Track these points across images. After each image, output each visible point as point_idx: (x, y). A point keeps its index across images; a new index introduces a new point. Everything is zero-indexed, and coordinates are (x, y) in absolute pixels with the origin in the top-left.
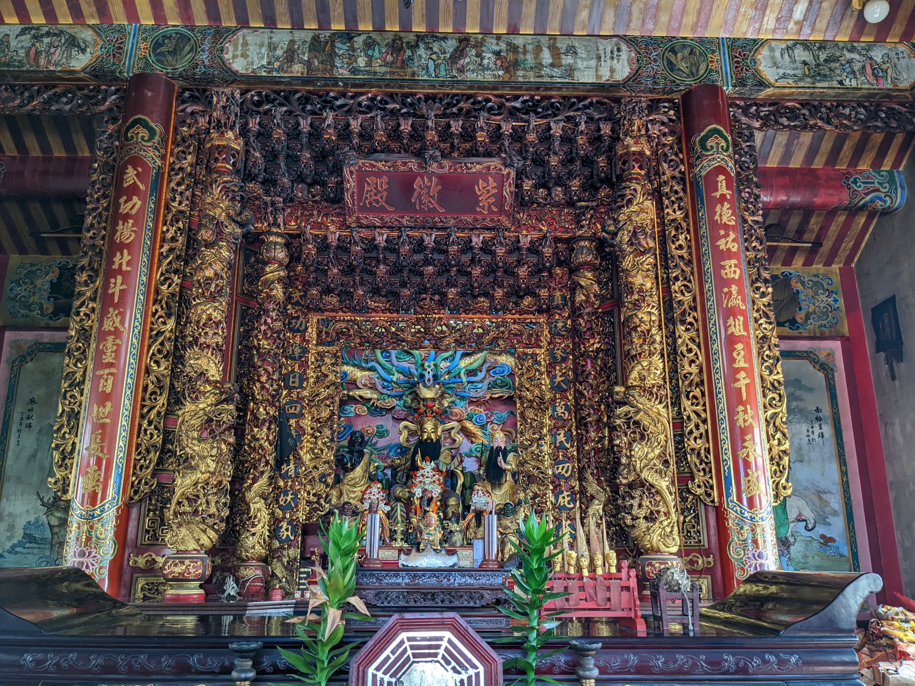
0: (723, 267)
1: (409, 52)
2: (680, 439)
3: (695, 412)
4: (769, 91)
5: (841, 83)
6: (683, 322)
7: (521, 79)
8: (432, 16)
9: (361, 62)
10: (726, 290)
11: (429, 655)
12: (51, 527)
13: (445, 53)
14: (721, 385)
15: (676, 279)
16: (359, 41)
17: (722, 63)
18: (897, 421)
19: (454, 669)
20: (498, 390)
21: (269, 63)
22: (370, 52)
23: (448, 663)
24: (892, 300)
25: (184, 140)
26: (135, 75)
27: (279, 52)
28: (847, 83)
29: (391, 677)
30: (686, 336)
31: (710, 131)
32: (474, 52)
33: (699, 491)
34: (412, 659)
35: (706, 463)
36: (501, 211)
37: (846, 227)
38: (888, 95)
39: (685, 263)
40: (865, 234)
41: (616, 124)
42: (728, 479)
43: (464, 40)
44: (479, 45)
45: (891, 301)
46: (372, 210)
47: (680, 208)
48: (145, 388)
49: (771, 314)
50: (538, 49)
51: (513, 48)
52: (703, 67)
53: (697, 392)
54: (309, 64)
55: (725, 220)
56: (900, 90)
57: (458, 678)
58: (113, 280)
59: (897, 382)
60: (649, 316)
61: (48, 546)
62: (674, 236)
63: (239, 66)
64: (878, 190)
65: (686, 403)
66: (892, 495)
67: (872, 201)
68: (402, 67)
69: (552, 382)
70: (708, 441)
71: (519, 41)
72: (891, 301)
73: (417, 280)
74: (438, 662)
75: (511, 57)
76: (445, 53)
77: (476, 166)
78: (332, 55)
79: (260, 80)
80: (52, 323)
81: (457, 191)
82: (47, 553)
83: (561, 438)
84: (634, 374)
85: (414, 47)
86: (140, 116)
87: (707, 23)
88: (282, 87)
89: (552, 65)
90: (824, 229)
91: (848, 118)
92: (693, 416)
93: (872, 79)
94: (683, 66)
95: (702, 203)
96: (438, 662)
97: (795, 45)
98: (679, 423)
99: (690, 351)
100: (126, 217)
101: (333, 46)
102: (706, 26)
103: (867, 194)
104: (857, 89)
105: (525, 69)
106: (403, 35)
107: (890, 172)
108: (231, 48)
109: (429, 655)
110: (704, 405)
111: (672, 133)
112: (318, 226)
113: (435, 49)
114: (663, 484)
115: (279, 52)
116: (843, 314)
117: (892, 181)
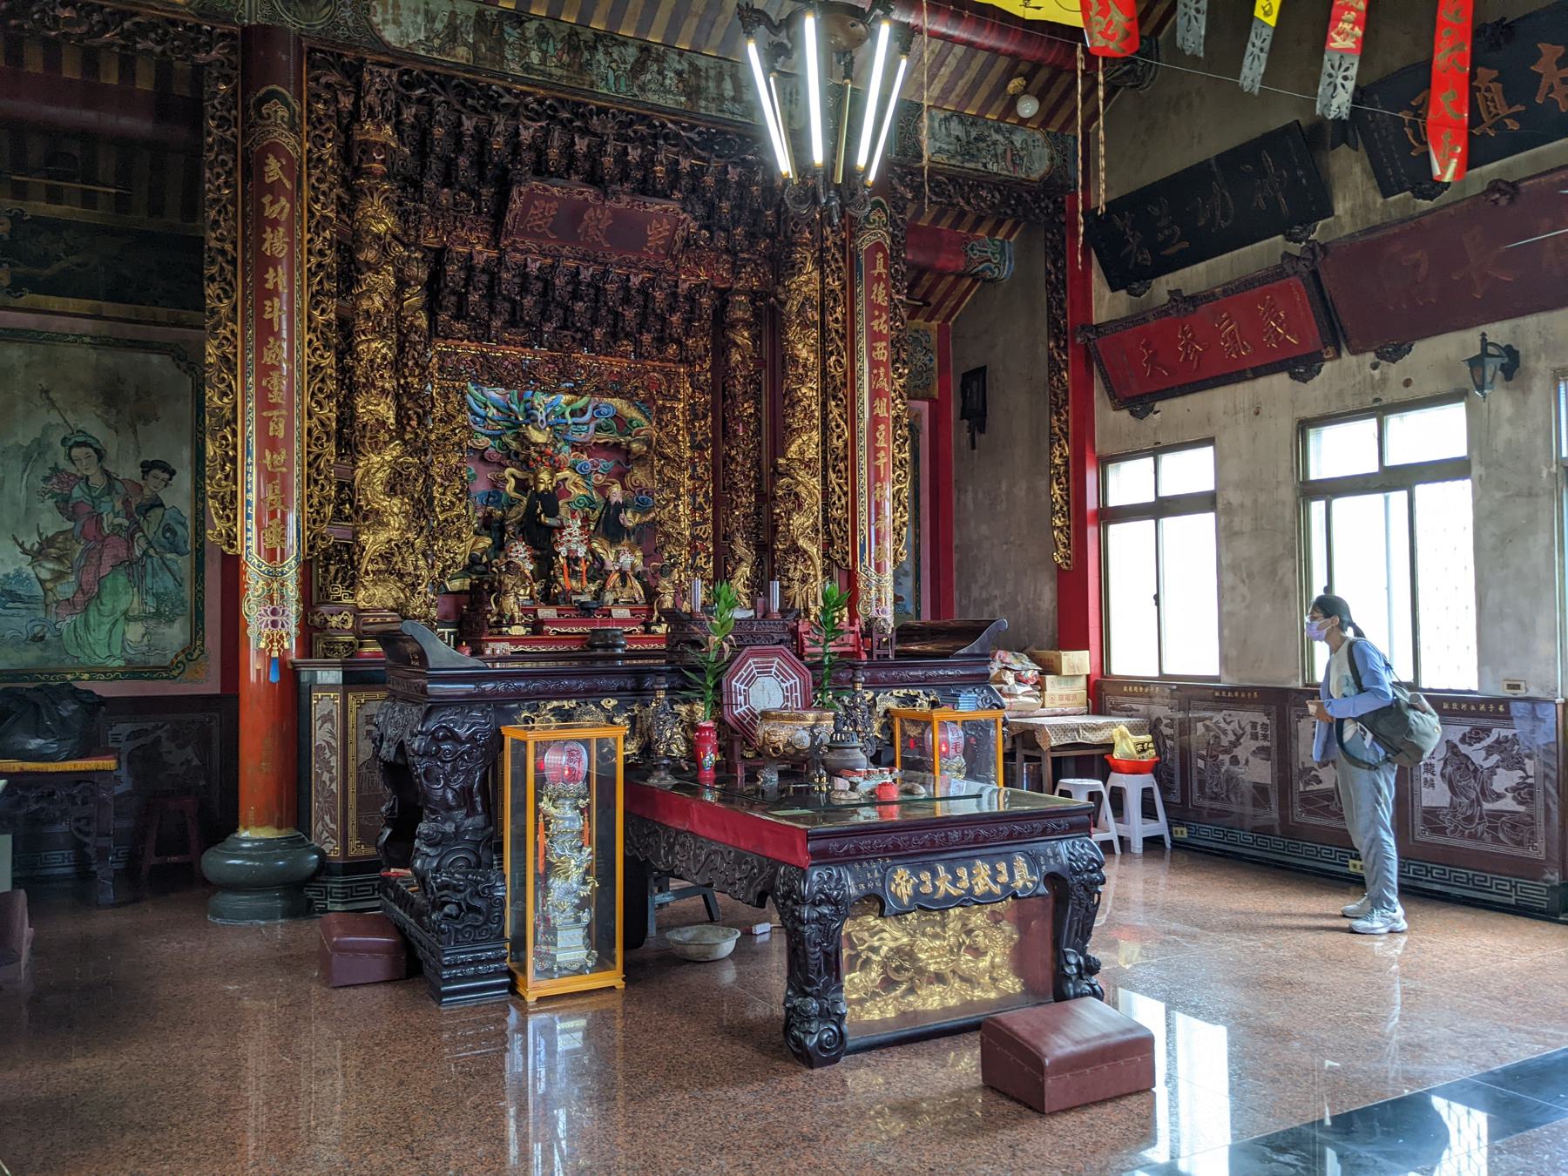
1: (586, 55)
2: (827, 505)
5: (985, 165)
6: (835, 398)
7: (702, 111)
8: (616, 15)
9: (535, 57)
12: (42, 582)
13: (625, 62)
14: (864, 462)
15: (832, 353)
16: (531, 27)
18: (970, 488)
20: (603, 434)
21: (427, 38)
22: (544, 46)
25: (319, 120)
26: (259, 25)
27: (439, 26)
32: (655, 68)
33: (838, 556)
36: (669, 254)
37: (953, 286)
38: (1020, 182)
39: (837, 340)
42: (862, 546)
43: (645, 49)
44: (660, 59)
45: (980, 373)
46: (532, 234)
48: (310, 431)
50: (720, 78)
51: (695, 70)
54: (474, 48)
58: (268, 303)
60: (809, 391)
61: (41, 606)
63: (390, 35)
65: (832, 476)
66: (955, 557)
68: (580, 73)
69: (693, 441)
71: (701, 63)
72: (980, 373)
73: (567, 318)
75: (693, 81)
76: (625, 62)
77: (655, 206)
78: (501, 41)
79: (417, 58)
80: (12, 302)
81: (627, 232)
82: (41, 614)
83: (700, 499)
84: (794, 448)
85: (593, 49)
86: (274, 87)
88: (437, 70)
89: (734, 99)
90: (933, 286)
91: (984, 200)
93: (1009, 164)
98: (826, 494)
100: (275, 224)
101: (502, 31)
105: (706, 99)
106: (579, 29)
107: (1002, 242)
108: (379, 9)
112: (465, 243)
113: (615, 56)
114: (813, 550)
115: (439, 26)
116: (936, 375)
117: (1002, 252)
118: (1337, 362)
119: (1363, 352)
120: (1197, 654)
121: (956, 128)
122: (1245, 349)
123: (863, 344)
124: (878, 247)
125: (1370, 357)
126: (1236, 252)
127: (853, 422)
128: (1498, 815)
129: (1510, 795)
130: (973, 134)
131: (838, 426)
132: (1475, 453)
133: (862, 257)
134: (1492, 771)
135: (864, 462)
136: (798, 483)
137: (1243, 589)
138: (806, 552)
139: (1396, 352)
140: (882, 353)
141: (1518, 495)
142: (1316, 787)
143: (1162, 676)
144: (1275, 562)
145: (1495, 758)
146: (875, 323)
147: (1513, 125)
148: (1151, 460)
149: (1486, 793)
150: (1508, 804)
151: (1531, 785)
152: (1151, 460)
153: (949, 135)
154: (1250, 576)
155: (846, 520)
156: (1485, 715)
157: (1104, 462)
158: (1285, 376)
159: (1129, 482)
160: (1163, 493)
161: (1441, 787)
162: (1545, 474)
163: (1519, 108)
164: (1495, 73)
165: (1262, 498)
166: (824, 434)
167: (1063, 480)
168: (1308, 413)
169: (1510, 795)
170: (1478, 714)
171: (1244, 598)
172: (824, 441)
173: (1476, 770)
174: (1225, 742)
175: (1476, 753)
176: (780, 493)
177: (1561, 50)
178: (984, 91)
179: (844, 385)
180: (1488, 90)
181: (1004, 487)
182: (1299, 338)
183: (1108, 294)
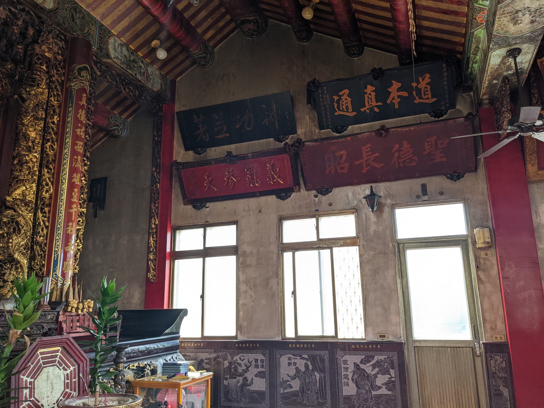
0: (77, 144)
2: (35, 232)
3: (43, 221)
4: (109, 61)
5: (136, 74)
6: (47, 167)
10: (76, 157)
11: (52, 362)
15: (48, 141)
17: (95, 32)
19: (64, 368)
23: (61, 365)
24: (106, 179)
28: (138, 76)
29: (31, 378)
30: (47, 175)
31: (85, 67)
34: (56, 363)
35: (43, 251)
39: (54, 134)
40: (99, 142)
41: (39, 32)
47: (57, 101)
49: (87, 176)
52: (87, 29)
53: (47, 209)
55: (82, 119)
56: (153, 91)
57: (66, 373)
59: (96, 219)
60: (34, 157)
62: (52, 115)
64: (118, 126)
65: (40, 215)
67: (114, 130)
70: (47, 239)
74: (56, 365)
87: (96, 8)
92: (42, 223)
94: (78, 21)
95: (72, 104)
96: (56, 365)
97: (124, 45)
98: (35, 225)
99: (47, 185)
102: (93, 9)
103: (114, 126)
104: (140, 81)
109: (52, 362)
110: (49, 218)
111: (62, 55)
117: (124, 125)
118: (298, 193)
119: (311, 190)
120: (222, 323)
121: (125, 52)
122: (257, 183)
123: (69, 140)
124: (84, 90)
125: (314, 192)
126: (260, 141)
127: (57, 183)
128: (379, 397)
129: (384, 387)
130: (132, 58)
131: (47, 185)
132: (361, 235)
133: (74, 93)
134: (376, 376)
135: (63, 208)
136: (19, 215)
137: (251, 292)
138: (18, 262)
139: (324, 191)
140: (80, 148)
141: (380, 253)
142: (289, 390)
143: (203, 337)
144: (268, 280)
145: (377, 369)
146: (78, 130)
147: (377, 110)
148: (202, 230)
149: (374, 387)
150: (384, 391)
151: (393, 381)
152: (202, 230)
153: (122, 53)
154: (255, 286)
155: (45, 244)
156: (372, 350)
157: (176, 229)
158: (274, 197)
159: (188, 239)
160: (207, 245)
161: (352, 385)
162: (391, 245)
163: (380, 104)
164: (374, 88)
165: (262, 249)
166: (38, 186)
167: (155, 236)
168: (285, 213)
169: (384, 387)
170: (368, 350)
171: (251, 297)
172: (38, 193)
173: (368, 376)
174: (240, 370)
175: (368, 368)
176: (5, 220)
177: (400, 85)
178: (141, 39)
179: (54, 161)
180: (370, 94)
181: (113, 238)
182: (283, 181)
183: (182, 151)
